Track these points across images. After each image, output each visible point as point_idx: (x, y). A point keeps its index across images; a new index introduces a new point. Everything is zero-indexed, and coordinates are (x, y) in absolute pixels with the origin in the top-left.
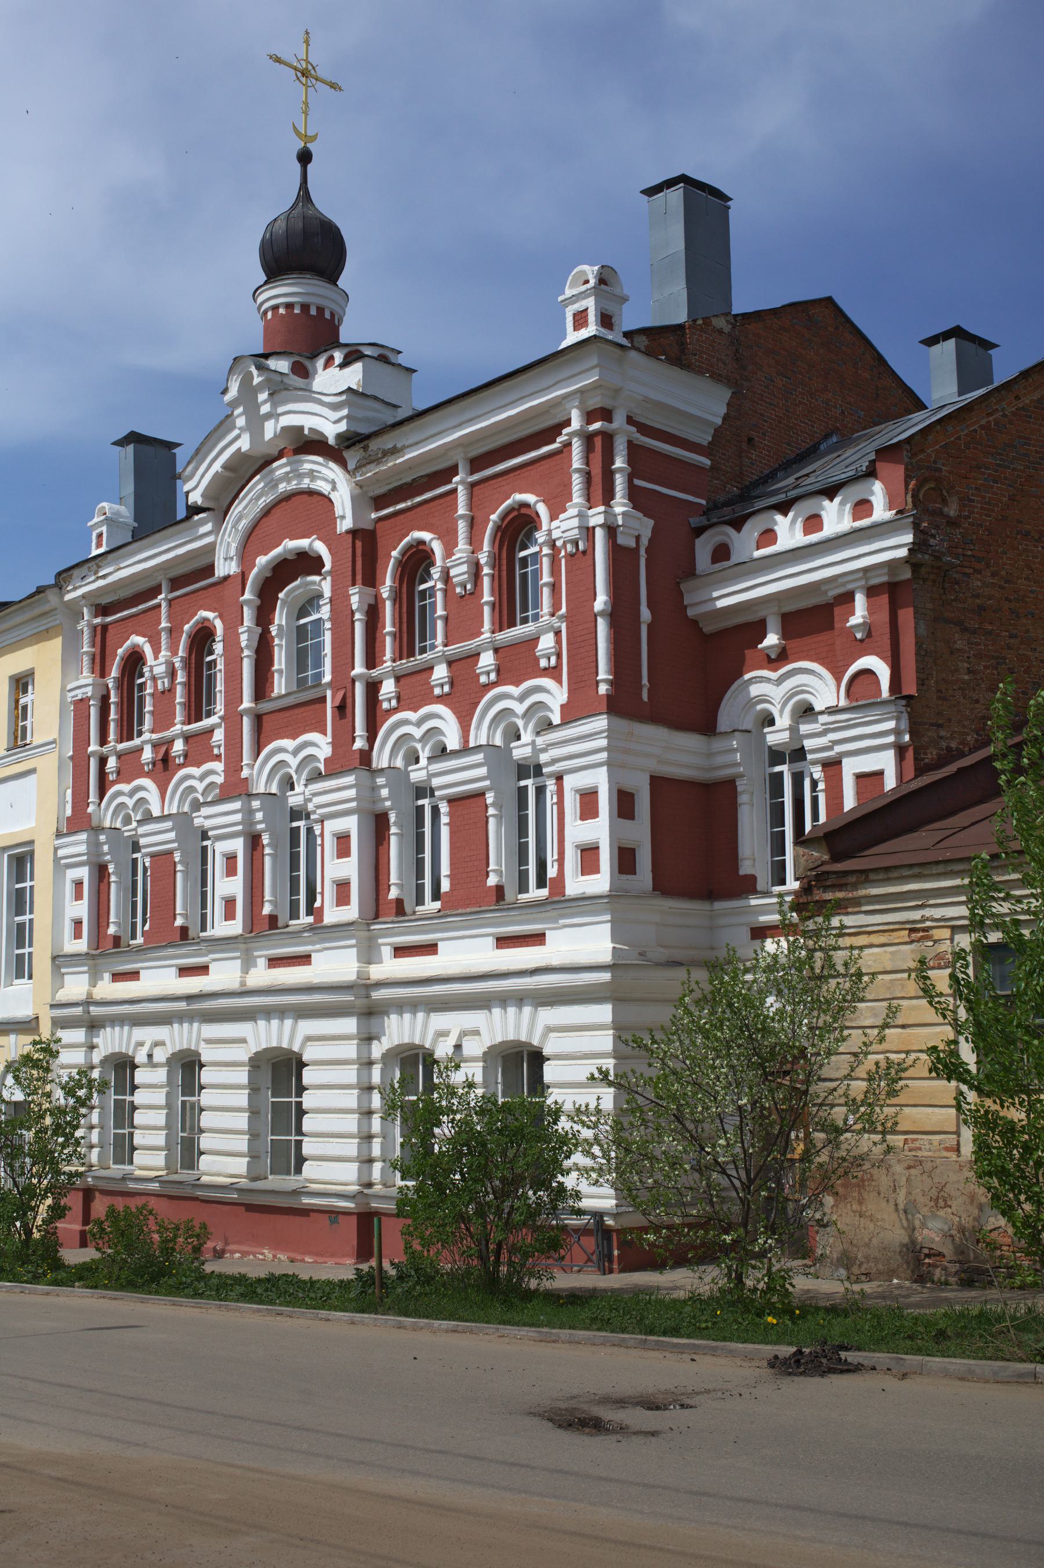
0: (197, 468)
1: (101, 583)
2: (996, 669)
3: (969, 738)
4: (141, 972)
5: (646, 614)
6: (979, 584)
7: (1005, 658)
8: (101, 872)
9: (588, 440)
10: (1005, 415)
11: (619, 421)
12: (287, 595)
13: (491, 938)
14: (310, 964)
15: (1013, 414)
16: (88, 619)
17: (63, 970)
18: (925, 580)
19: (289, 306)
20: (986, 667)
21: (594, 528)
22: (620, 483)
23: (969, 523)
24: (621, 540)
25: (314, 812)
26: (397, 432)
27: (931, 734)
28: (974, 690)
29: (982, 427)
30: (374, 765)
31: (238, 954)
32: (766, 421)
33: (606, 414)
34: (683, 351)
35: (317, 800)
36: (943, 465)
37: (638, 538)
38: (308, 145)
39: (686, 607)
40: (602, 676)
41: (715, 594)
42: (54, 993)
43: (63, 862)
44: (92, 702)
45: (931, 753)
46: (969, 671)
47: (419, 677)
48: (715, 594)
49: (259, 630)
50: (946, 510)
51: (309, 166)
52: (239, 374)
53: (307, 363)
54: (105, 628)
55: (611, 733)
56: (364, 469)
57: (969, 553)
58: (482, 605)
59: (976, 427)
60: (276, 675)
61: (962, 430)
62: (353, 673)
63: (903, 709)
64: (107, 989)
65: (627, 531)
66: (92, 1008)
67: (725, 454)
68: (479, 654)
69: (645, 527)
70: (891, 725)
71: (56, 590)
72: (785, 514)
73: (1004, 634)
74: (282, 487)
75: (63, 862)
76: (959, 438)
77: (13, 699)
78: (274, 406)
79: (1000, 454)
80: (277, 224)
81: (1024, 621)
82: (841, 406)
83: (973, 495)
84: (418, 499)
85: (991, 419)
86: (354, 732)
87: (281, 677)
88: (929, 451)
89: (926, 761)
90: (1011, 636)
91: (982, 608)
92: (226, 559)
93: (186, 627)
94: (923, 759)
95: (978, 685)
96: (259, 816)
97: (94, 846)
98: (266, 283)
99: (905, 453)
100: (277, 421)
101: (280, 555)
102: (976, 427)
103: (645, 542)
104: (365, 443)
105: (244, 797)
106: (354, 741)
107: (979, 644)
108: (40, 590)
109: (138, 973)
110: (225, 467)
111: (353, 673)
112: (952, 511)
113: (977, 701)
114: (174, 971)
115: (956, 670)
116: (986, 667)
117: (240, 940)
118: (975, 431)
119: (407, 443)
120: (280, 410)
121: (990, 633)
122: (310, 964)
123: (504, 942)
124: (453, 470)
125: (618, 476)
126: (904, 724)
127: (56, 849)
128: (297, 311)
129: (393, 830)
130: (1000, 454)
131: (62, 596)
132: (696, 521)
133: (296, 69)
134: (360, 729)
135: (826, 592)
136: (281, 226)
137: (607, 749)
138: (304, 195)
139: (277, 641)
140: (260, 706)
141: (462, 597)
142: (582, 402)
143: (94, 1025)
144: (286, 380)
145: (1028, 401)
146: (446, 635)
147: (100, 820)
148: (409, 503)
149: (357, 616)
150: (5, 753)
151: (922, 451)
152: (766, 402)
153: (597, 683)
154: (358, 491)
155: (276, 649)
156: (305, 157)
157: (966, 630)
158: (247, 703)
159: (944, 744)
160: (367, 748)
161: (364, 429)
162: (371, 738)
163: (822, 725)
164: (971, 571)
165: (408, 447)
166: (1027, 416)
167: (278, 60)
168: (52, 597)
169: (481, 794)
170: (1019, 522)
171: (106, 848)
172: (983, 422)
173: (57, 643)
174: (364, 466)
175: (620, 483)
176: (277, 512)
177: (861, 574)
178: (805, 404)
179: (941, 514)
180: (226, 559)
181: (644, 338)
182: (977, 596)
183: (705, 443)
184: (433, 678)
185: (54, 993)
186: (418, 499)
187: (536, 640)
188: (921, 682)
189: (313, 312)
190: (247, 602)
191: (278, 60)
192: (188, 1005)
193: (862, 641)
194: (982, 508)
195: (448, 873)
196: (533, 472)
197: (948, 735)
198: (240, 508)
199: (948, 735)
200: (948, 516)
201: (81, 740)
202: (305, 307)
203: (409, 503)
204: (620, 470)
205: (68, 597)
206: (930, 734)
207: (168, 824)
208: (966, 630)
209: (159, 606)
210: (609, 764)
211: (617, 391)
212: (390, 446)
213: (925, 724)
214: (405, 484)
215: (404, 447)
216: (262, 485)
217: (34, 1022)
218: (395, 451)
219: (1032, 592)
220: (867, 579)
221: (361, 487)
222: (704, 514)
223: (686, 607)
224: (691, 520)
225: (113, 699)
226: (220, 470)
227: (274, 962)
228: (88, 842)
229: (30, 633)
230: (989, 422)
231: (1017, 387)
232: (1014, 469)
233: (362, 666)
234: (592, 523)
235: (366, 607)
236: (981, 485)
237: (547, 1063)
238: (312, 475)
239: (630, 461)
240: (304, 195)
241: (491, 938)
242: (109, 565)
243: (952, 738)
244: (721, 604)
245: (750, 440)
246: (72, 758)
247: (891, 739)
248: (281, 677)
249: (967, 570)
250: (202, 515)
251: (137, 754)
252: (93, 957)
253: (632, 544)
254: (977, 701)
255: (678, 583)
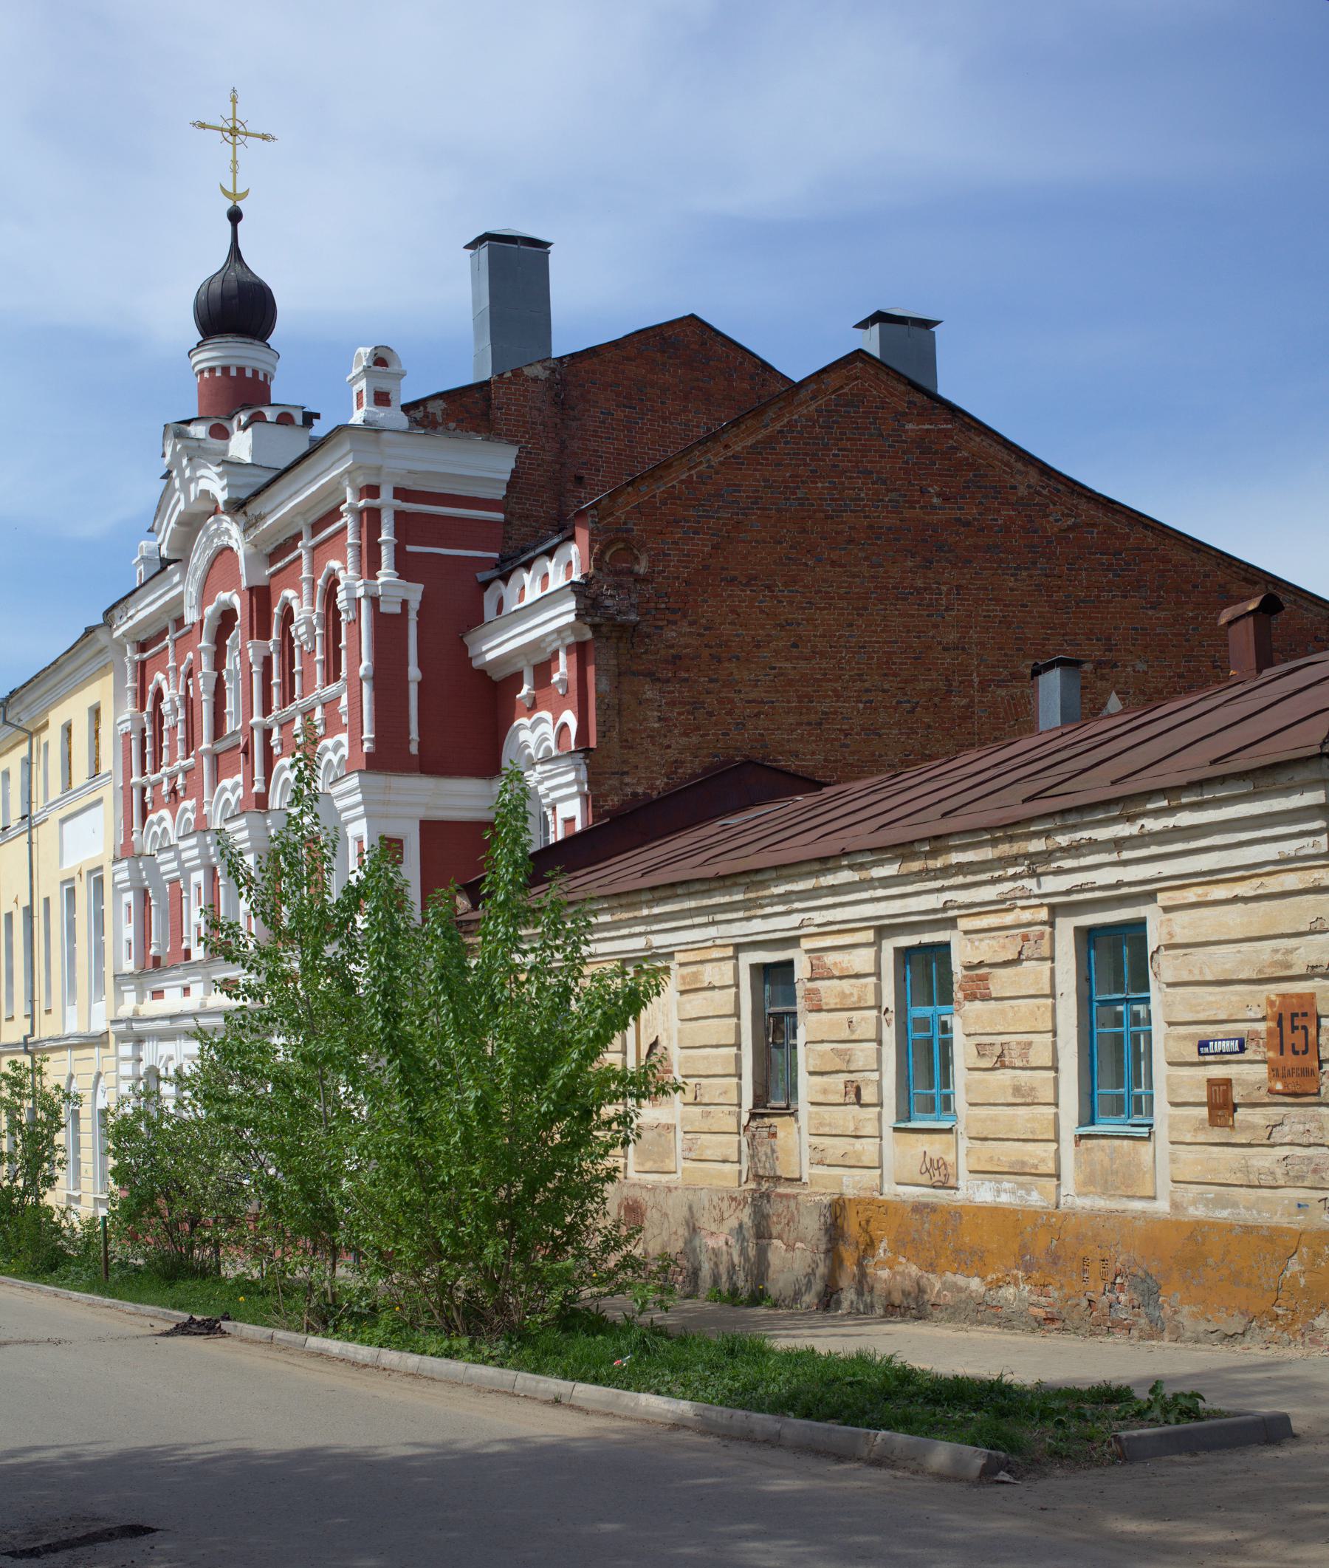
0: (161, 524)
1: (131, 623)
2: (693, 714)
3: (658, 782)
4: (165, 991)
5: (414, 673)
6: (674, 634)
7: (703, 703)
8: (144, 896)
9: (359, 513)
10: (710, 467)
11: (386, 496)
12: (233, 642)
15: (721, 463)
16: (131, 655)
17: (123, 988)
18: (608, 638)
19: (212, 370)
20: (679, 714)
21: (360, 599)
22: (386, 555)
23: (663, 578)
24: (383, 609)
25: (546, 796)
27: (614, 782)
28: (665, 736)
29: (682, 482)
30: (270, 807)
31: (200, 978)
32: (601, 457)
33: (372, 491)
34: (489, 406)
35: (549, 784)
36: (635, 525)
37: (405, 604)
38: (238, 204)
39: (471, 659)
40: (366, 735)
41: (484, 648)
42: (116, 1008)
43: (119, 886)
44: (132, 736)
45: (612, 800)
46: (660, 719)
48: (484, 648)
49: (216, 674)
50: (637, 567)
51: (240, 225)
53: (226, 424)
54: (143, 664)
55: (363, 787)
57: (663, 606)
59: (674, 483)
60: (228, 717)
61: (658, 488)
62: (251, 722)
63: (582, 761)
64: (151, 1007)
65: (388, 599)
66: (134, 1025)
67: (538, 501)
69: (414, 593)
70: (571, 776)
71: (106, 629)
72: (529, 572)
73: (702, 679)
75: (119, 886)
76: (654, 496)
77: (93, 729)
78: (194, 470)
79: (703, 505)
80: (212, 286)
81: (727, 665)
82: (705, 424)
83: (668, 549)
84: (287, 559)
85: (693, 472)
86: (253, 776)
88: (618, 514)
89: (607, 807)
90: (711, 681)
91: (677, 657)
94: (603, 806)
95: (670, 731)
97: (135, 872)
98: (199, 345)
99: (590, 519)
100: (197, 484)
102: (674, 483)
103: (414, 606)
105: (199, 833)
106: (253, 784)
107: (673, 692)
108: (89, 631)
109: (162, 992)
110: (178, 523)
111: (251, 722)
112: (642, 568)
113: (669, 747)
115: (645, 719)
116: (679, 714)
117: (198, 965)
118: (674, 487)
119: (267, 510)
121: (686, 680)
124: (298, 536)
125: (383, 548)
126: (583, 775)
127: (114, 874)
128: (218, 374)
130: (703, 505)
131: (112, 634)
132: (482, 576)
133: (222, 130)
134: (258, 776)
135: (545, 649)
136: (217, 287)
137: (364, 802)
138: (235, 253)
139: (227, 686)
140: (215, 747)
142: (352, 482)
143: (139, 1040)
144: (202, 444)
145: (739, 449)
146: (302, 690)
147: (143, 848)
149: (255, 668)
150: (87, 781)
151: (612, 514)
152: (601, 437)
153: (362, 742)
154: (253, 550)
156: (235, 216)
157: (659, 680)
158: (205, 745)
159: (629, 790)
160: (263, 790)
161: (243, 495)
162: (267, 783)
163: (540, 773)
164: (665, 623)
165: (269, 513)
166: (738, 463)
167: (203, 126)
168: (101, 636)
170: (723, 569)
171: (144, 873)
172: (684, 477)
173: (110, 679)
175: (386, 555)
176: (216, 564)
177: (555, 636)
178: (657, 431)
179: (630, 572)
181: (441, 402)
182: (672, 647)
183: (500, 498)
185: (116, 1008)
186: (287, 559)
188: (602, 735)
189: (233, 373)
190: (204, 648)
191: (203, 126)
193: (564, 696)
194: (678, 561)
197: (635, 781)
198: (195, 560)
199: (635, 781)
200: (637, 574)
201: (128, 773)
202: (226, 370)
204: (386, 542)
205: (116, 634)
206: (611, 782)
208: (659, 680)
210: (367, 815)
211: (379, 469)
213: (605, 773)
217: (105, 1036)
219: (738, 636)
220: (563, 639)
221: (256, 546)
222: (497, 566)
223: (471, 659)
224: (478, 575)
225: (148, 733)
228: (129, 868)
229: (95, 669)
230: (691, 476)
231: (725, 436)
232: (719, 518)
233: (258, 715)
234: (358, 596)
235: (261, 660)
236: (680, 538)
239: (397, 533)
240: (235, 253)
243: (638, 783)
244: (490, 656)
245: (579, 479)
246: (122, 788)
247: (574, 789)
249: (660, 623)
250: (172, 566)
252: (138, 976)
253: (398, 610)
254: (669, 747)
255: (462, 638)
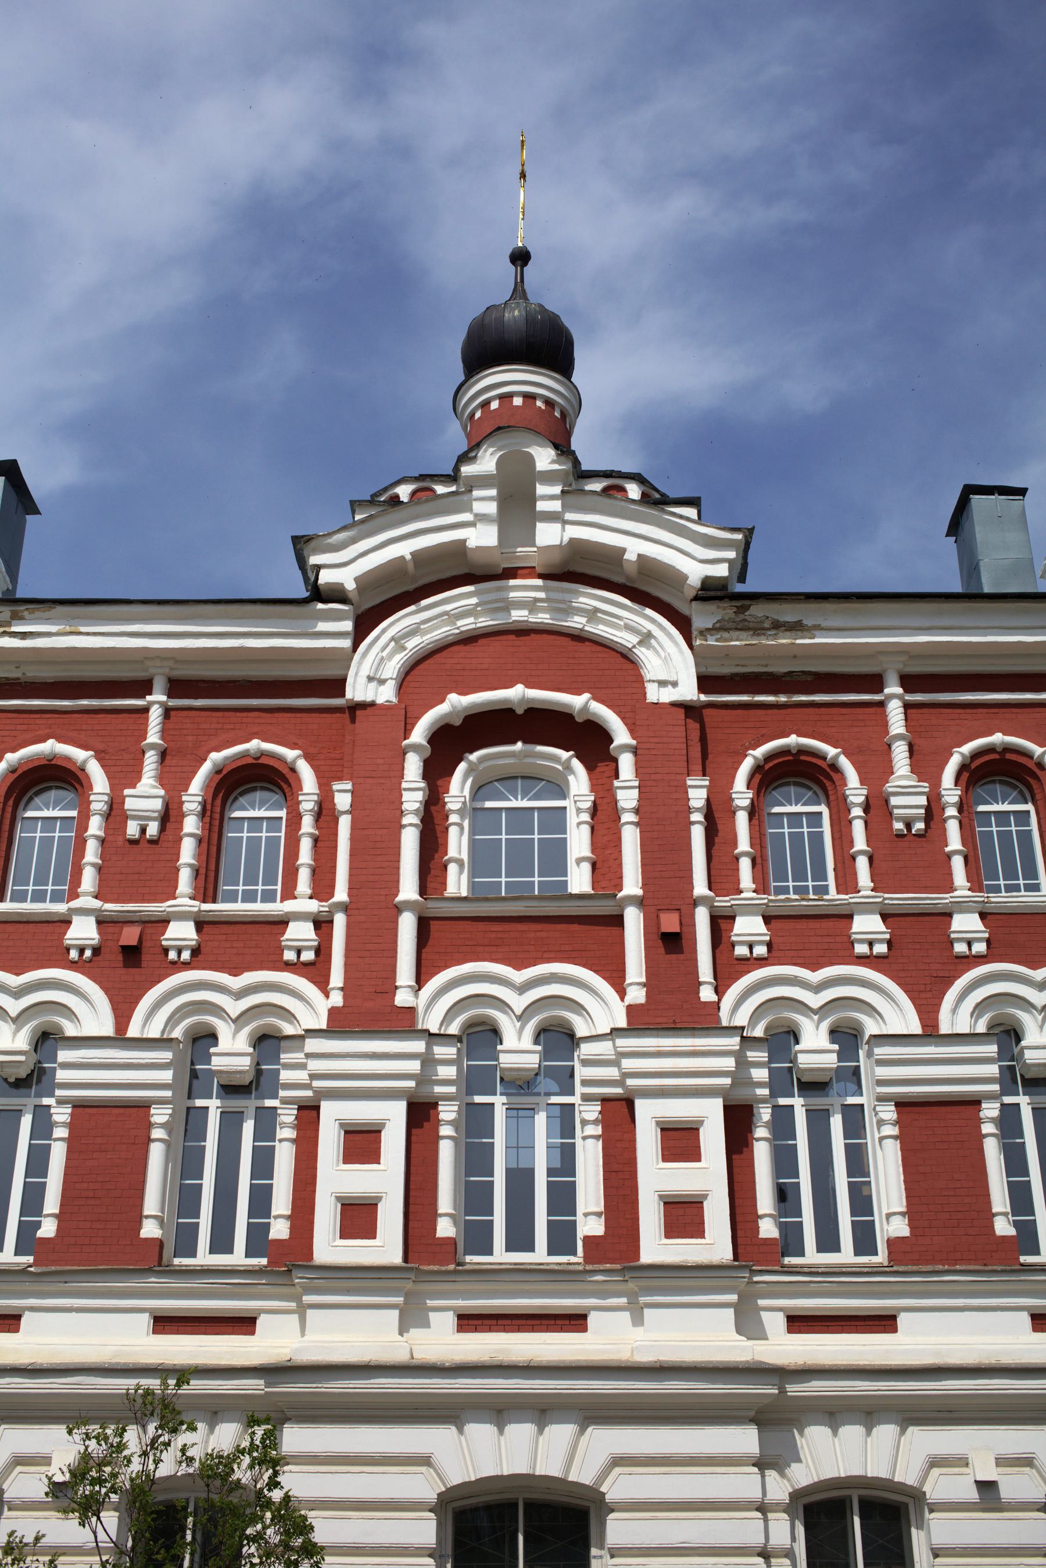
0: (354, 541)
12: (481, 760)
13: (147, 1315)
14: (253, 1333)
26: (813, 606)
47: (49, 928)
52: (499, 449)
56: (726, 635)
58: (949, 857)
68: (168, 922)
74: (518, 615)
87: (461, 872)
92: (370, 679)
93: (216, 757)
96: (448, 1072)
101: (506, 701)
104: (747, 602)
114: (145, 1320)
119: (824, 624)
120: (569, 516)
122: (253, 1333)
123: (164, 1323)
129: (761, 1132)
140: (430, 904)
141: (900, 836)
148: (783, 699)
155: (453, 831)
165: (823, 629)
169: (974, 1103)
174: (727, 630)
176: (495, 644)
180: (370, 679)
184: (286, 936)
187: (65, 922)
192: (268, 1385)
195: (288, 1212)
196: (1023, 715)
203: (783, 699)
207: (166, 1056)
209: (145, 710)
212: (790, 618)
214: (771, 674)
215: (818, 628)
216: (474, 600)
218: (797, 627)
226: (631, 556)
227: (468, 1322)
237: (612, 1516)
238: (593, 614)
241: (147, 1315)
242: (48, 620)
248: (461, 872)
251: (276, 929)
